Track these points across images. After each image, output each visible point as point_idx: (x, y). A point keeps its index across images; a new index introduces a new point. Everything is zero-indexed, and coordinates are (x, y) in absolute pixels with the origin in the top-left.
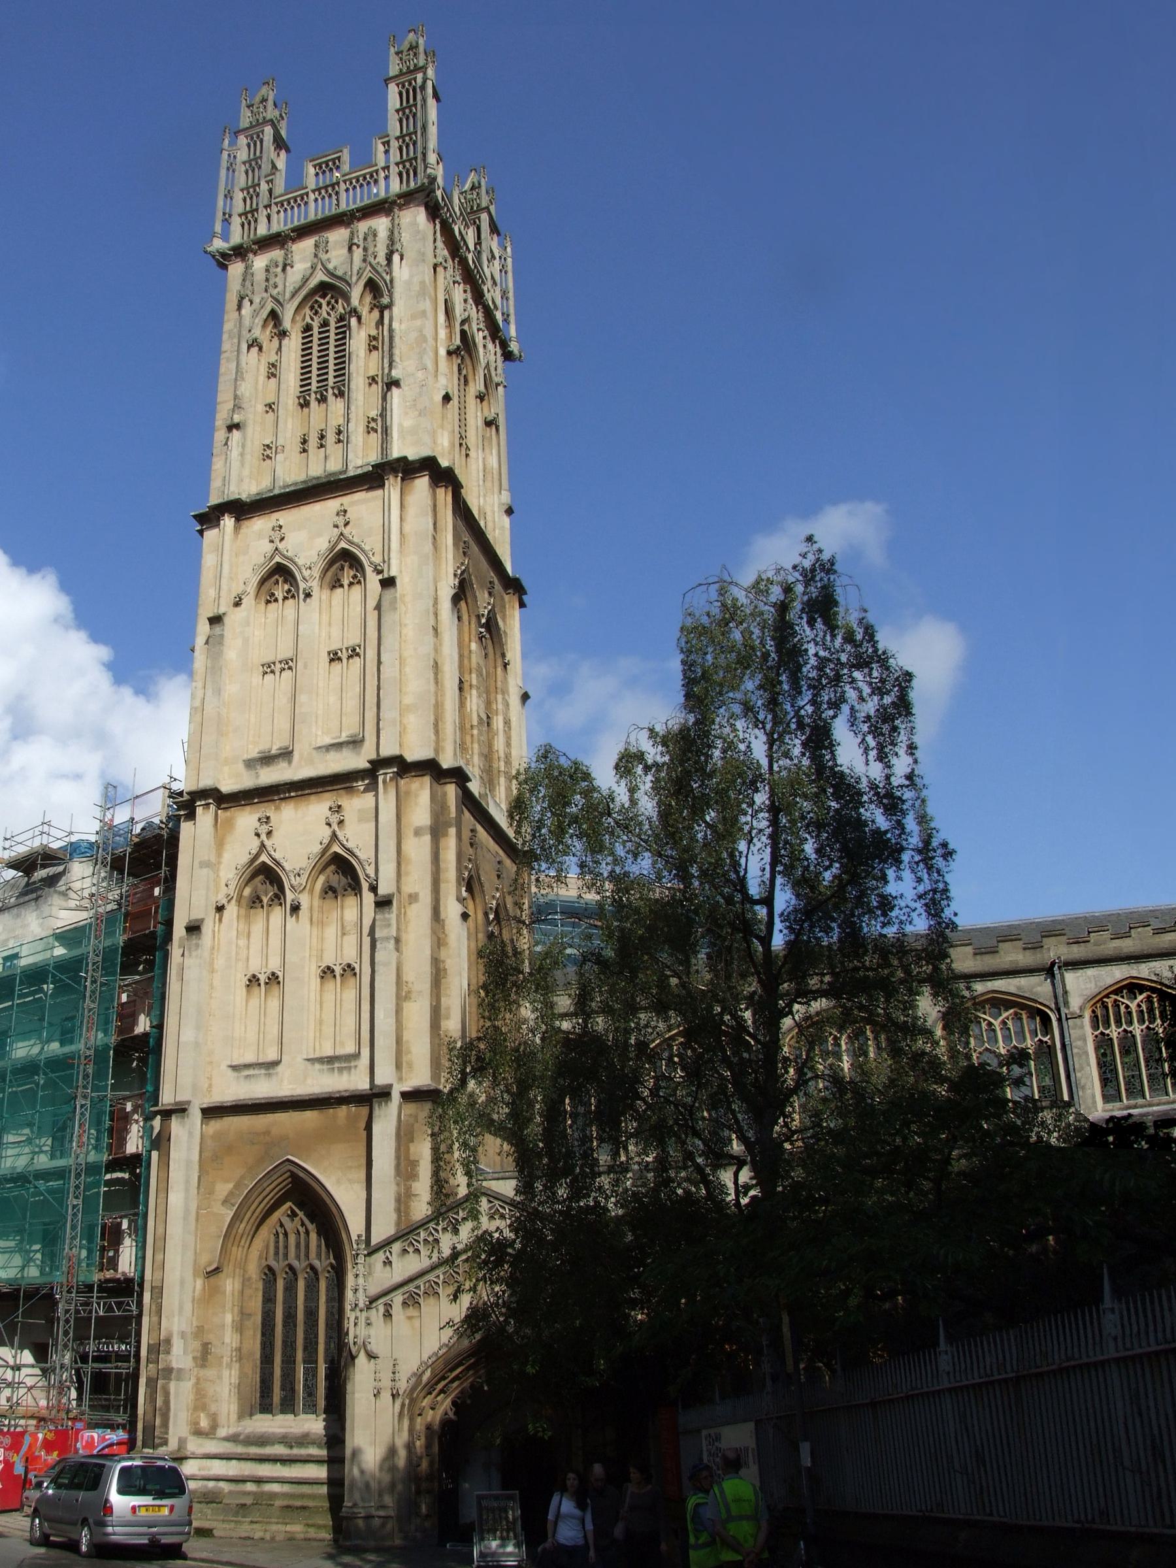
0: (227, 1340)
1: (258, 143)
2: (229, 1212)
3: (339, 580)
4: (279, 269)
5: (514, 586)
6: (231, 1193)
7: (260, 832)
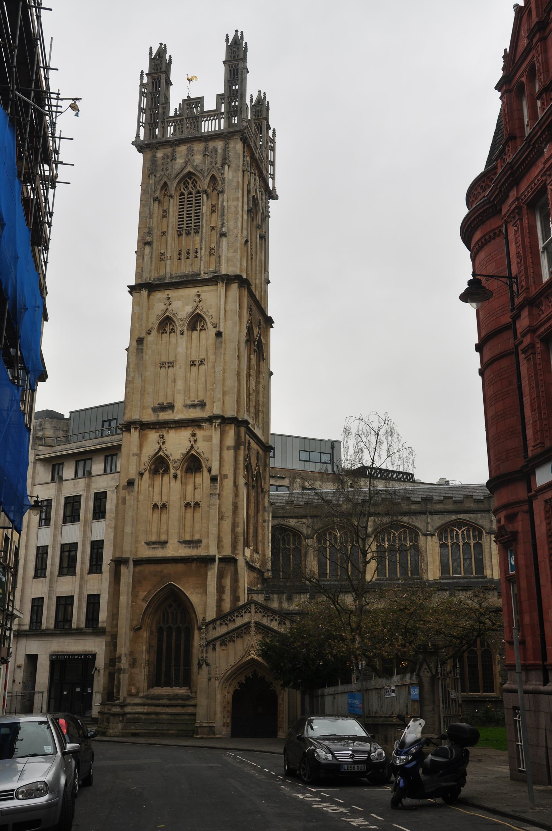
0: (144, 657)
6: (146, 596)
7: (159, 442)
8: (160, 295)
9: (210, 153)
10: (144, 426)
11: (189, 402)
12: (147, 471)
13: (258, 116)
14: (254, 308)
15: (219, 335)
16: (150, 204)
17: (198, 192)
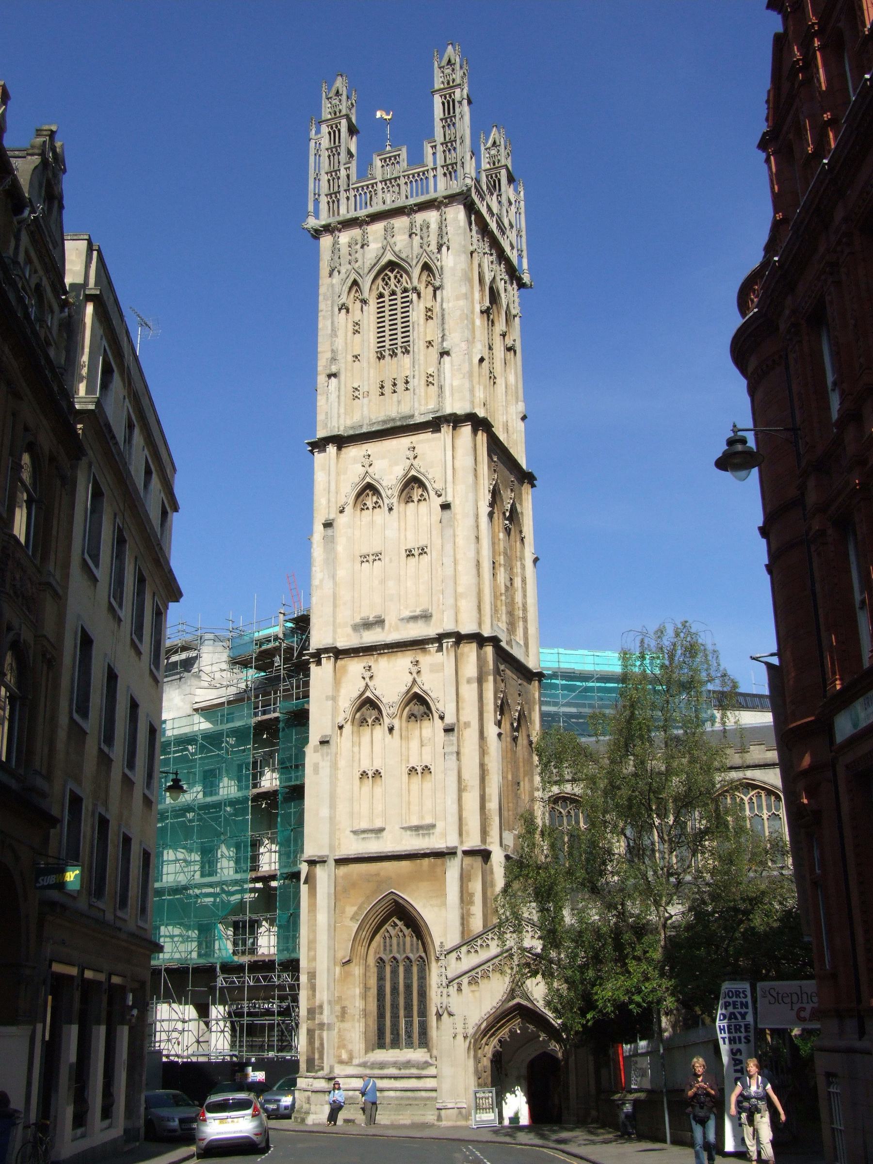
0: (357, 1005)
1: (337, 132)
2: (354, 924)
3: (411, 497)
4: (358, 246)
5: (527, 478)
6: (356, 913)
7: (365, 676)
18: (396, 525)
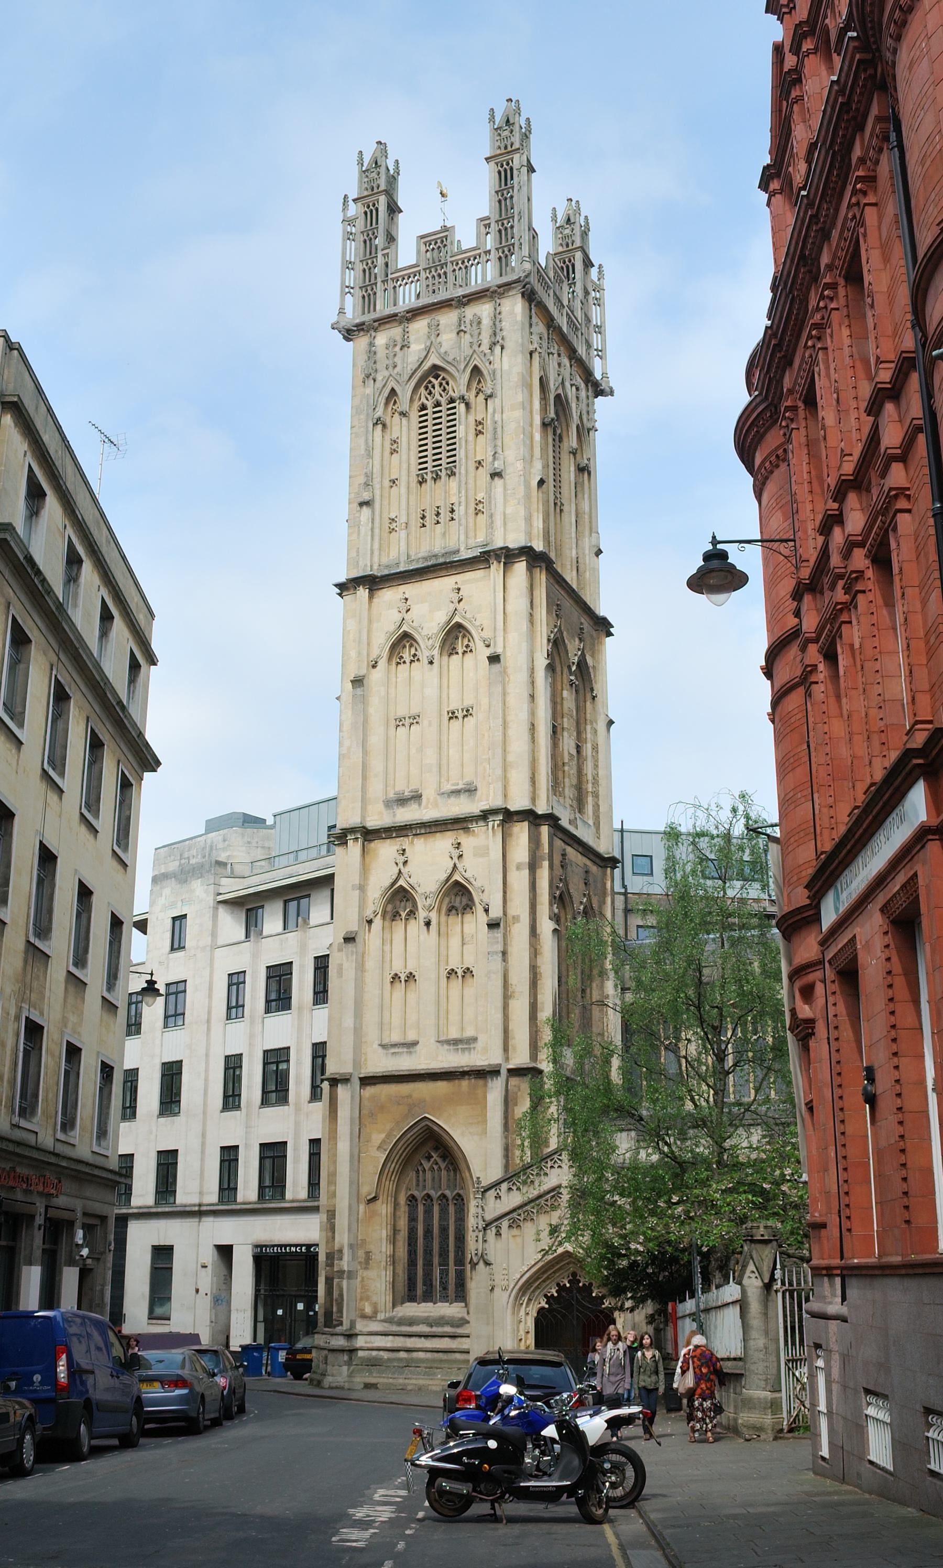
1: (374, 212)
3: (454, 648)
6: (384, 1142)
8: (389, 596)
9: (469, 326)
10: (369, 835)
11: (448, 787)
12: (379, 915)
13: (567, 245)
14: (567, 603)
15: (494, 659)
16: (367, 431)
17: (452, 401)
18: (436, 681)
